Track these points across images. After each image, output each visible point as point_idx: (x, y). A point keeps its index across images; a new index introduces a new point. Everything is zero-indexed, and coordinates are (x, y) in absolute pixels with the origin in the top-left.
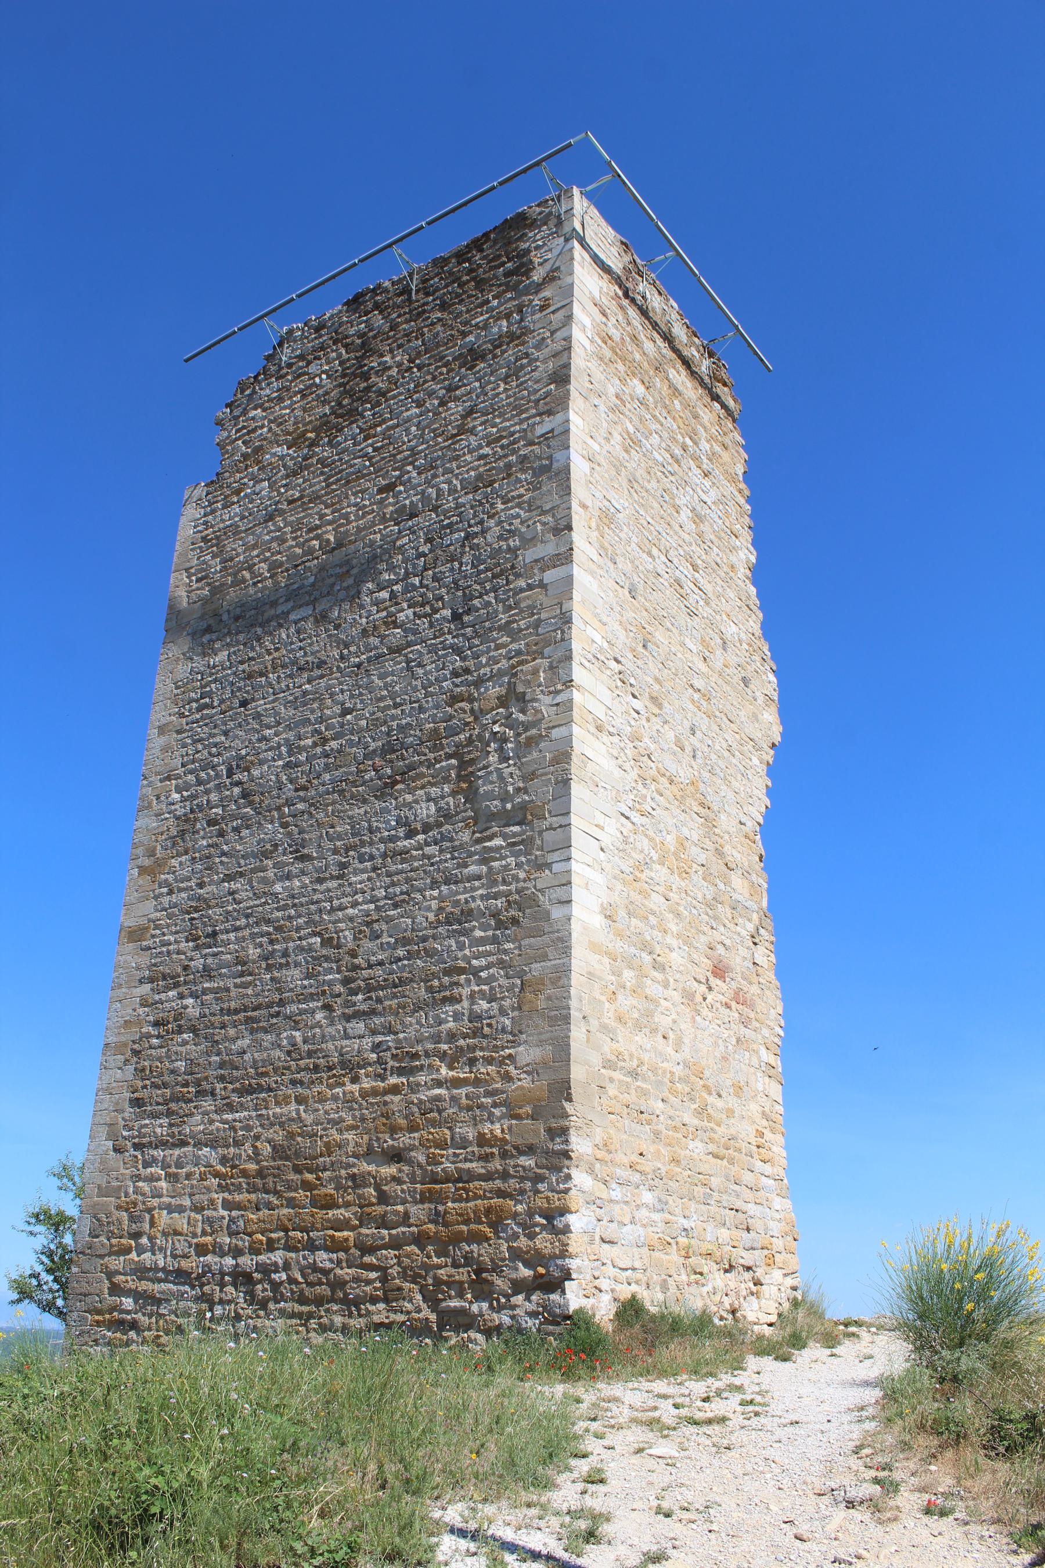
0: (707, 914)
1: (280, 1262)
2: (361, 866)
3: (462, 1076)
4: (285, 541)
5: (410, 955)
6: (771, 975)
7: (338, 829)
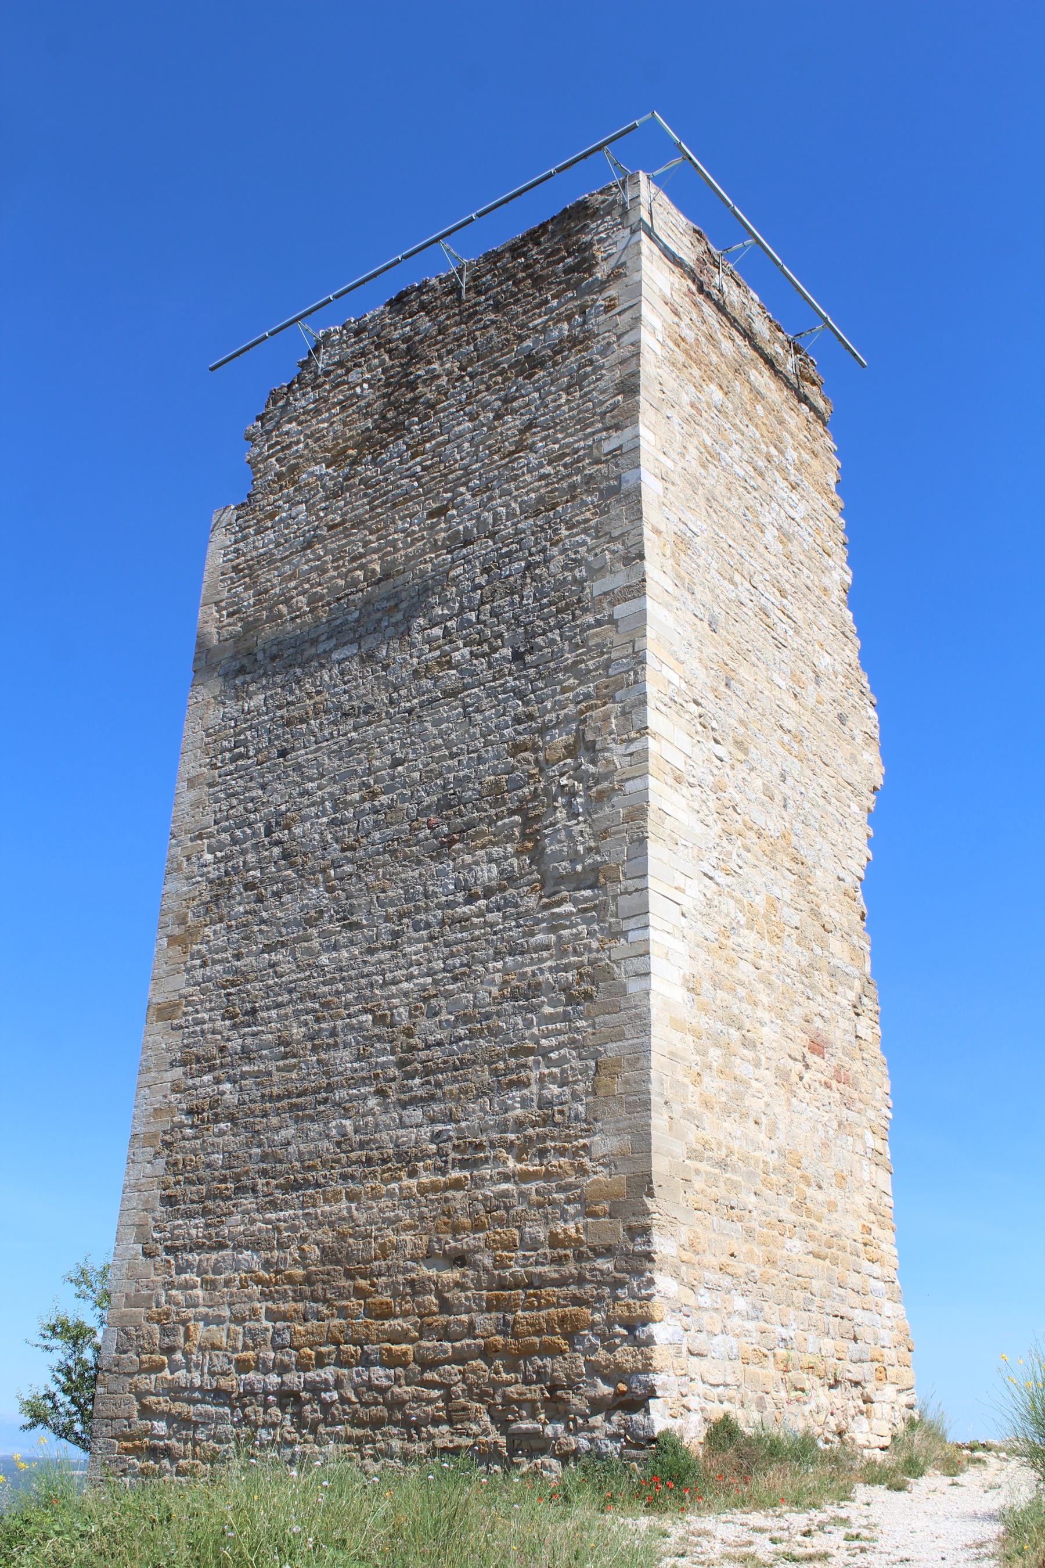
1: (331, 1379)
2: (416, 935)
3: (531, 1169)
4: (326, 571)
5: (472, 1035)
6: (877, 1050)
7: (390, 893)
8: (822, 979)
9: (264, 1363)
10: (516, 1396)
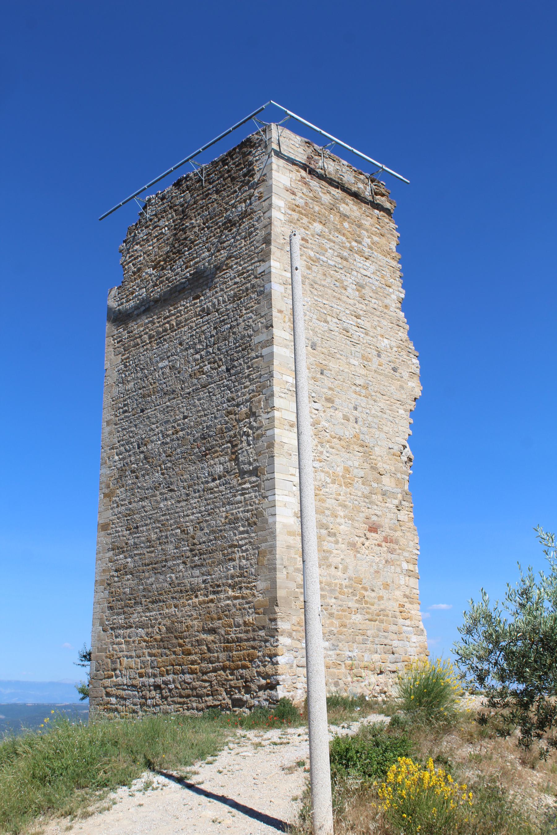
0: (365, 502)
1: (171, 680)
2: (194, 495)
3: (237, 595)
4: (154, 324)
5: (215, 539)
6: (411, 524)
7: (184, 477)
9: (148, 674)
10: (233, 685)
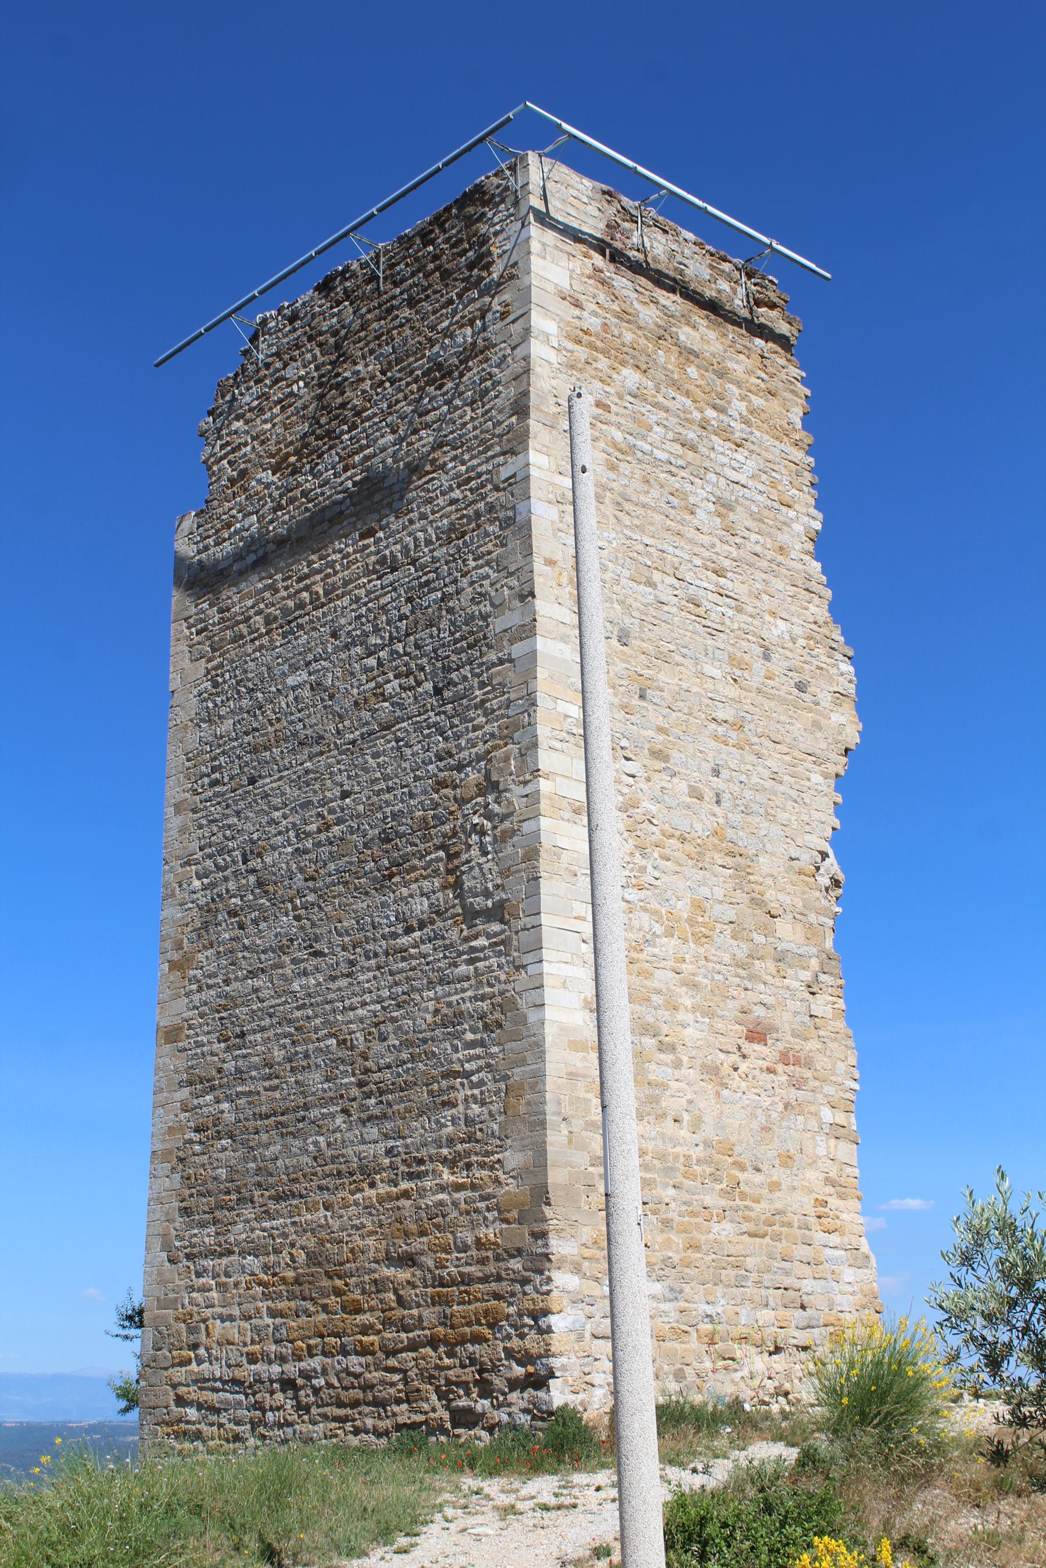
0: (738, 976)
1: (319, 1369)
2: (367, 964)
3: (460, 1181)
4: (277, 591)
5: (413, 1058)
6: (841, 1025)
8: (765, 967)
